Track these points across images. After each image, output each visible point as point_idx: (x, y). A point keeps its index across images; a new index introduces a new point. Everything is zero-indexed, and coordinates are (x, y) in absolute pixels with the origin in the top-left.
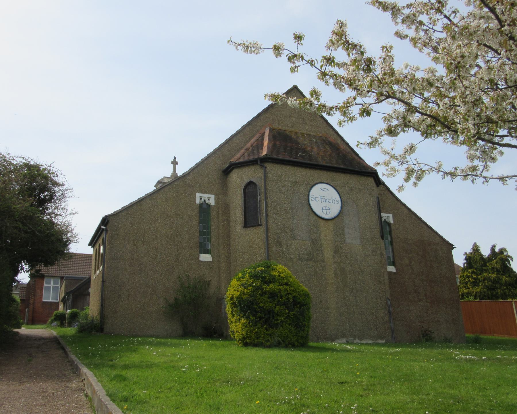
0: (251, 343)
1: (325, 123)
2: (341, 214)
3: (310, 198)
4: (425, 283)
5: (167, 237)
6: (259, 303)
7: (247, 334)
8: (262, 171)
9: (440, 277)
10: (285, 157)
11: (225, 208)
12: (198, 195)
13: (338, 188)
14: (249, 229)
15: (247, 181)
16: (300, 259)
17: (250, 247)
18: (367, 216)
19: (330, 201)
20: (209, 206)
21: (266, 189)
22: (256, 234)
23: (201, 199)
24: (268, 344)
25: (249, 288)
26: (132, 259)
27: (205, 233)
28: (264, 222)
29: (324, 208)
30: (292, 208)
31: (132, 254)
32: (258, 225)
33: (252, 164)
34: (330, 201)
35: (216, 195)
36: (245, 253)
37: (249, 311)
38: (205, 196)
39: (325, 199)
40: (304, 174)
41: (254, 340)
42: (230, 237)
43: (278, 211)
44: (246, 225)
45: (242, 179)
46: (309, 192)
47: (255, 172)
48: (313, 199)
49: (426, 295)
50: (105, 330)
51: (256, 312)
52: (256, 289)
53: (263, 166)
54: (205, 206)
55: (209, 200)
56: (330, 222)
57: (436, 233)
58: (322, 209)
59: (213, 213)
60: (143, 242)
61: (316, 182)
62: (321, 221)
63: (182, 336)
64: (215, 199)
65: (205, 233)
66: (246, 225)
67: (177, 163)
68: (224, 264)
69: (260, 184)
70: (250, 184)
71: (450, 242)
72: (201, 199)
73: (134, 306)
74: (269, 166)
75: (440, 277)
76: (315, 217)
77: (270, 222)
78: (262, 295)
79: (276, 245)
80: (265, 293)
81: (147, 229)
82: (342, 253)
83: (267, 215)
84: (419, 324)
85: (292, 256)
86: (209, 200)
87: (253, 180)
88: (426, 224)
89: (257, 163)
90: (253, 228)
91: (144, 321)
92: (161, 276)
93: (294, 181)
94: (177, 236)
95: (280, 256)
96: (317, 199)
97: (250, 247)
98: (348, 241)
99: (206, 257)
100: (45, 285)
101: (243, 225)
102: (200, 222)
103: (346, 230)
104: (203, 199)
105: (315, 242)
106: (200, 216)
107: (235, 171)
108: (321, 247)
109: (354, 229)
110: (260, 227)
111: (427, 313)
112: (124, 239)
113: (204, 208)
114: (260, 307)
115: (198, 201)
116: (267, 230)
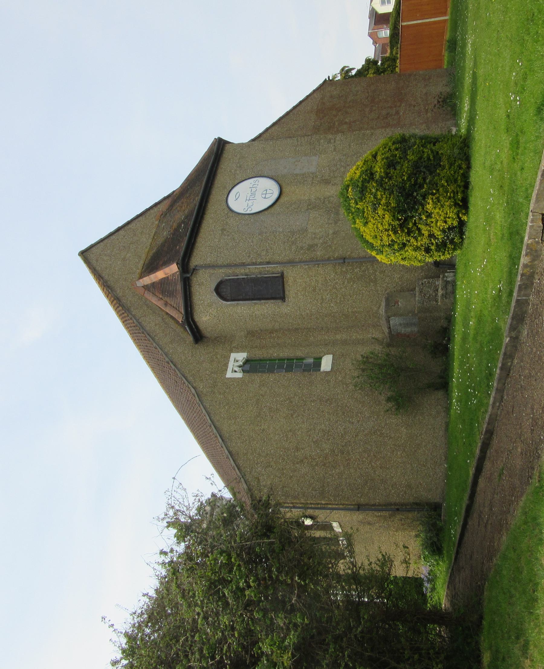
0: (463, 192)
1: (141, 218)
2: (274, 178)
3: (248, 212)
4: (374, 108)
5: (292, 415)
6: (403, 180)
7: (450, 198)
8: (201, 272)
9: (368, 92)
10: (184, 245)
11: (253, 336)
12: (229, 374)
13: (237, 181)
14: (287, 293)
16: (336, 223)
17: (314, 290)
18: (279, 150)
19: (254, 190)
21: (229, 266)
22: (296, 280)
23: (235, 372)
24: (464, 166)
25: (379, 197)
26: (324, 465)
27: (289, 365)
28: (279, 269)
29: (264, 196)
30: (261, 234)
31: (317, 465)
32: (281, 279)
33: (190, 289)
34: (254, 190)
35: (231, 351)
36: (322, 299)
37: (415, 194)
39: (250, 196)
40: (211, 221)
41: (460, 187)
42: (297, 329)
43: (263, 250)
45: (210, 305)
46: (239, 214)
47: (202, 283)
48: (250, 209)
49: (391, 107)
50: (437, 500)
51: (416, 183)
52: (381, 186)
53: (194, 269)
54: (247, 367)
55: (237, 361)
56: (284, 190)
57: (308, 97)
58: (265, 198)
59: (259, 354)
60: (297, 449)
61: (225, 207)
63: (447, 391)
64: (238, 352)
65: (289, 365)
68: (337, 336)
69: (221, 274)
70: (220, 290)
71: (321, 82)
72: (235, 372)
73: (399, 460)
74: (196, 261)
75: (368, 92)
76: (276, 206)
77: (277, 258)
78: (390, 178)
79: (314, 250)
80: (387, 174)
81: (277, 444)
82: (329, 176)
83: (268, 263)
84: (429, 114)
85: (331, 232)
86: (237, 361)
87: (214, 286)
88: (295, 108)
89: (188, 278)
90: (286, 286)
91: (424, 444)
92: (353, 423)
93: (220, 232)
94: (291, 402)
95: (330, 246)
96: (250, 204)
97: (314, 290)
98: (313, 169)
99: (327, 363)
101: (279, 302)
102: (271, 370)
103: (297, 171)
104: (237, 369)
105: (312, 206)
106: (263, 372)
107: (197, 318)
108: (320, 199)
109: (296, 163)
110: (285, 274)
111: (414, 106)
112: (291, 477)
113: (250, 366)
114: (409, 179)
115: (239, 375)
116: (291, 263)
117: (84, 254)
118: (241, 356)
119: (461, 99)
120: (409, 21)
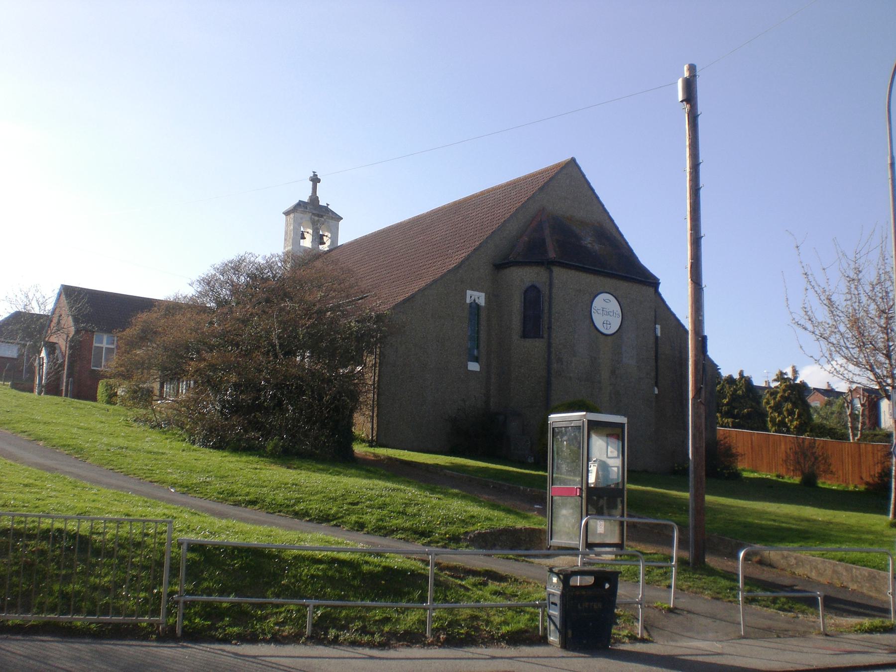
12: (469, 292)
15: (528, 284)
20: (478, 306)
22: (536, 346)
28: (546, 336)
32: (537, 335)
38: (476, 294)
39: (607, 313)
44: (525, 335)
59: (483, 315)
62: (601, 336)
66: (525, 335)
67: (319, 181)
69: (545, 290)
99: (474, 366)
100: (95, 344)
113: (475, 307)
115: (468, 301)
116: (549, 345)
117: (573, 160)
118: (482, 301)
119: (393, 482)
120: (502, 470)
